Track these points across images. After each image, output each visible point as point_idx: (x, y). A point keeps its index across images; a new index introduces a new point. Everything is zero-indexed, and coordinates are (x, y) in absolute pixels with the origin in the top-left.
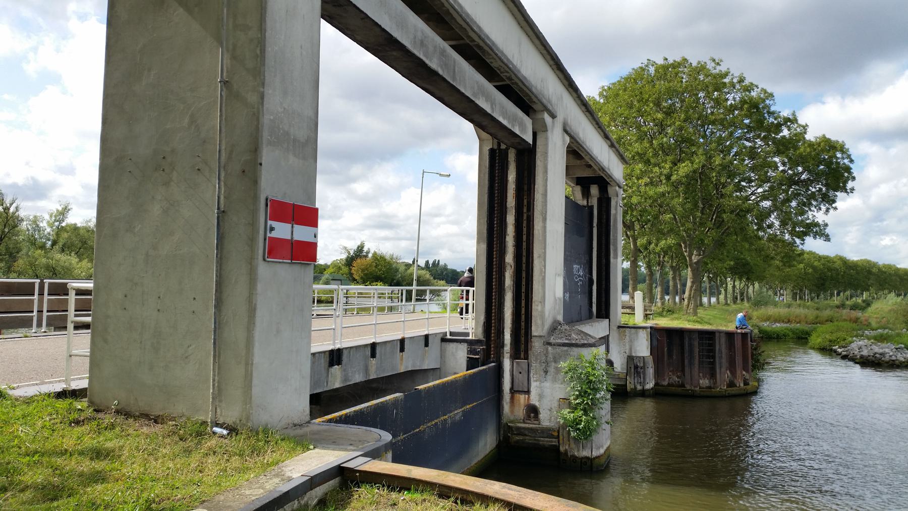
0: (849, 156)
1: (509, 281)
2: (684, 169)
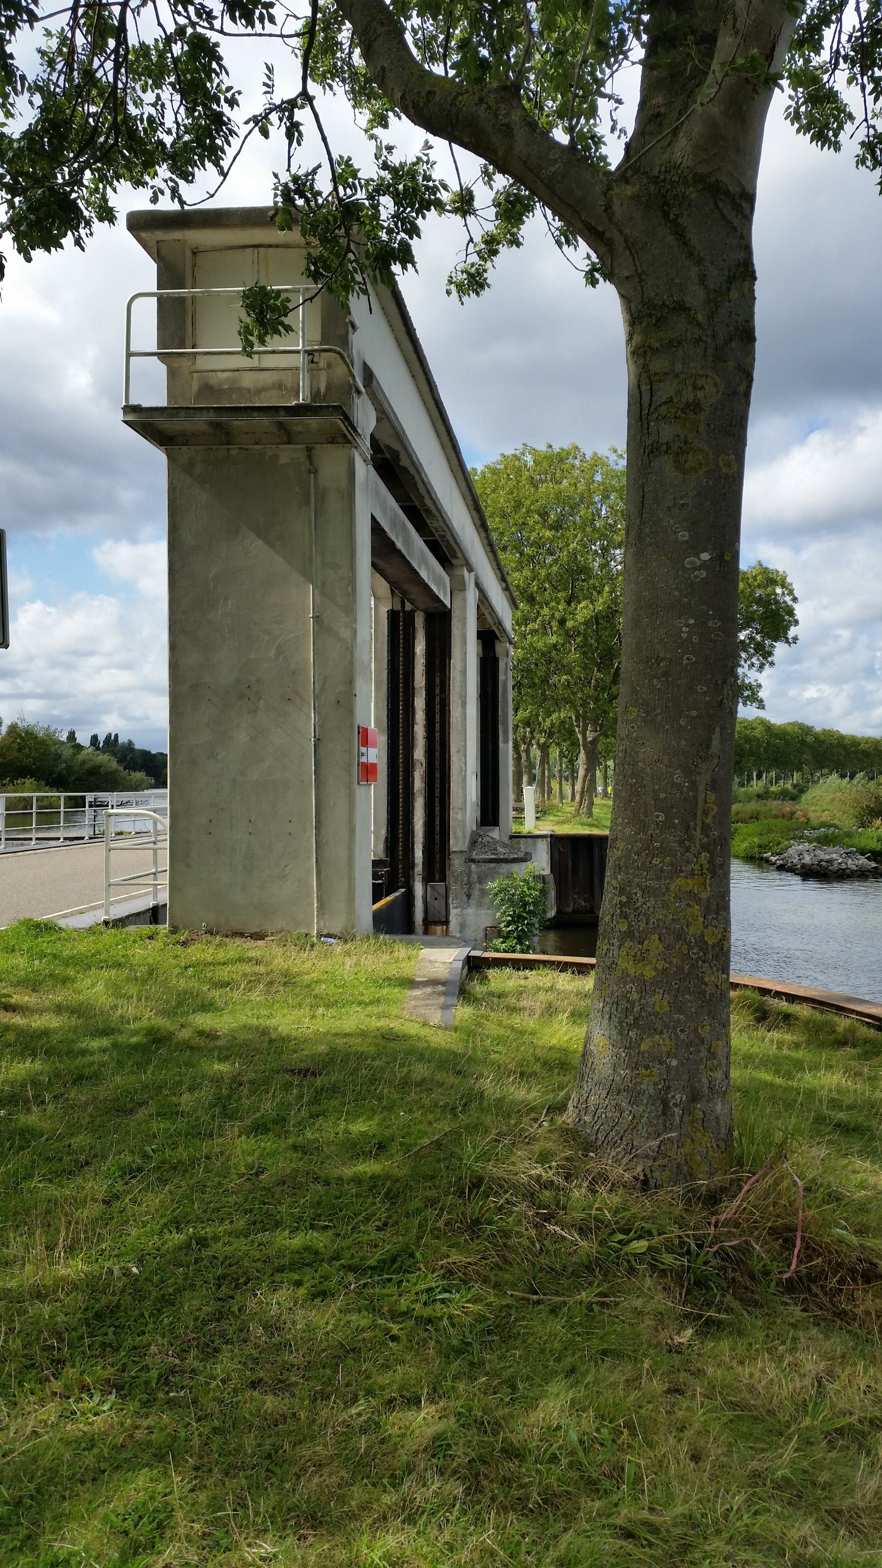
0: (791, 592)
1: (418, 783)
2: (583, 611)
